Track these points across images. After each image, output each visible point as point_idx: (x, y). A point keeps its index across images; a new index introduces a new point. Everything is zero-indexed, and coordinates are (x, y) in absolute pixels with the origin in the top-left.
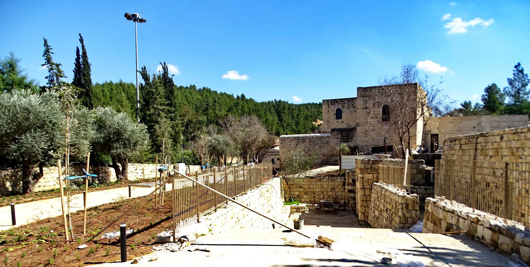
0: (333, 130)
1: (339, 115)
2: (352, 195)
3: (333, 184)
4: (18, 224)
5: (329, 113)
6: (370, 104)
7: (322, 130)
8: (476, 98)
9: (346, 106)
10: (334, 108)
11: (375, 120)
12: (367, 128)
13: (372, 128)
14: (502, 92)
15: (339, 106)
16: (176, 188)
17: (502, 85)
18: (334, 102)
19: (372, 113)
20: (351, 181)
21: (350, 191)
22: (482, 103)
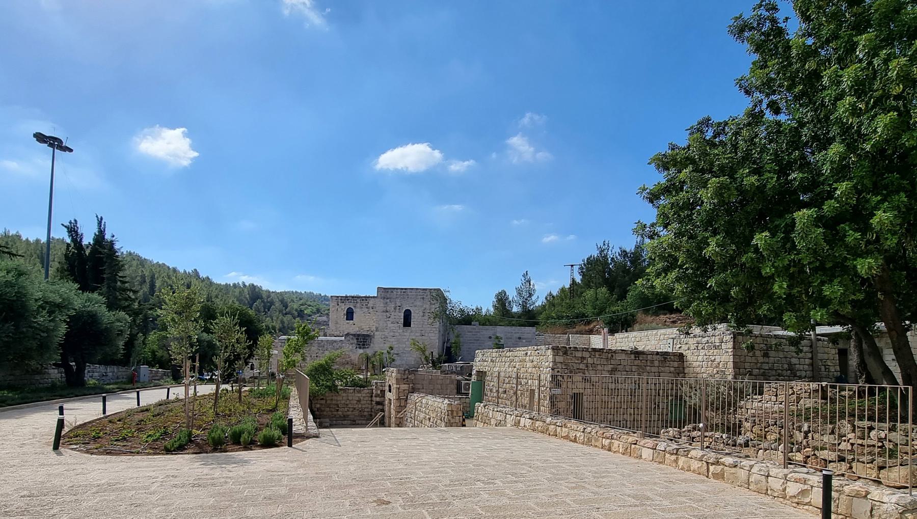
0: (348, 335)
1: (350, 315)
2: (380, 407)
3: (359, 395)
4: (107, 414)
5: (337, 315)
6: (391, 307)
7: (328, 332)
8: (487, 306)
9: (358, 305)
10: (344, 307)
11: (396, 325)
12: (386, 334)
13: (392, 334)
14: (511, 299)
15: (351, 306)
16: (100, 405)
17: (512, 294)
18: (345, 299)
19: (392, 317)
20: (379, 392)
21: (378, 403)
22: (492, 309)
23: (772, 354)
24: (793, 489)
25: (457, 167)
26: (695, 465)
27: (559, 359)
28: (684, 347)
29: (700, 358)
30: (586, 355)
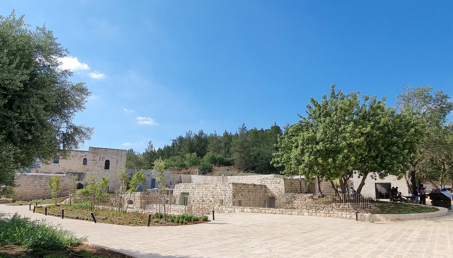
11: (100, 168)
23: (292, 185)
24: (348, 216)
25: (96, 76)
26: (323, 215)
27: (235, 188)
28: (266, 183)
29: (272, 187)
30: (241, 186)
